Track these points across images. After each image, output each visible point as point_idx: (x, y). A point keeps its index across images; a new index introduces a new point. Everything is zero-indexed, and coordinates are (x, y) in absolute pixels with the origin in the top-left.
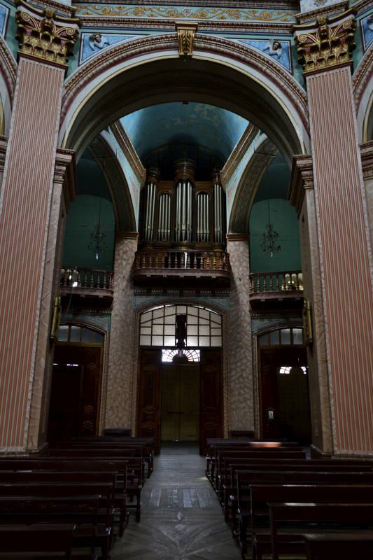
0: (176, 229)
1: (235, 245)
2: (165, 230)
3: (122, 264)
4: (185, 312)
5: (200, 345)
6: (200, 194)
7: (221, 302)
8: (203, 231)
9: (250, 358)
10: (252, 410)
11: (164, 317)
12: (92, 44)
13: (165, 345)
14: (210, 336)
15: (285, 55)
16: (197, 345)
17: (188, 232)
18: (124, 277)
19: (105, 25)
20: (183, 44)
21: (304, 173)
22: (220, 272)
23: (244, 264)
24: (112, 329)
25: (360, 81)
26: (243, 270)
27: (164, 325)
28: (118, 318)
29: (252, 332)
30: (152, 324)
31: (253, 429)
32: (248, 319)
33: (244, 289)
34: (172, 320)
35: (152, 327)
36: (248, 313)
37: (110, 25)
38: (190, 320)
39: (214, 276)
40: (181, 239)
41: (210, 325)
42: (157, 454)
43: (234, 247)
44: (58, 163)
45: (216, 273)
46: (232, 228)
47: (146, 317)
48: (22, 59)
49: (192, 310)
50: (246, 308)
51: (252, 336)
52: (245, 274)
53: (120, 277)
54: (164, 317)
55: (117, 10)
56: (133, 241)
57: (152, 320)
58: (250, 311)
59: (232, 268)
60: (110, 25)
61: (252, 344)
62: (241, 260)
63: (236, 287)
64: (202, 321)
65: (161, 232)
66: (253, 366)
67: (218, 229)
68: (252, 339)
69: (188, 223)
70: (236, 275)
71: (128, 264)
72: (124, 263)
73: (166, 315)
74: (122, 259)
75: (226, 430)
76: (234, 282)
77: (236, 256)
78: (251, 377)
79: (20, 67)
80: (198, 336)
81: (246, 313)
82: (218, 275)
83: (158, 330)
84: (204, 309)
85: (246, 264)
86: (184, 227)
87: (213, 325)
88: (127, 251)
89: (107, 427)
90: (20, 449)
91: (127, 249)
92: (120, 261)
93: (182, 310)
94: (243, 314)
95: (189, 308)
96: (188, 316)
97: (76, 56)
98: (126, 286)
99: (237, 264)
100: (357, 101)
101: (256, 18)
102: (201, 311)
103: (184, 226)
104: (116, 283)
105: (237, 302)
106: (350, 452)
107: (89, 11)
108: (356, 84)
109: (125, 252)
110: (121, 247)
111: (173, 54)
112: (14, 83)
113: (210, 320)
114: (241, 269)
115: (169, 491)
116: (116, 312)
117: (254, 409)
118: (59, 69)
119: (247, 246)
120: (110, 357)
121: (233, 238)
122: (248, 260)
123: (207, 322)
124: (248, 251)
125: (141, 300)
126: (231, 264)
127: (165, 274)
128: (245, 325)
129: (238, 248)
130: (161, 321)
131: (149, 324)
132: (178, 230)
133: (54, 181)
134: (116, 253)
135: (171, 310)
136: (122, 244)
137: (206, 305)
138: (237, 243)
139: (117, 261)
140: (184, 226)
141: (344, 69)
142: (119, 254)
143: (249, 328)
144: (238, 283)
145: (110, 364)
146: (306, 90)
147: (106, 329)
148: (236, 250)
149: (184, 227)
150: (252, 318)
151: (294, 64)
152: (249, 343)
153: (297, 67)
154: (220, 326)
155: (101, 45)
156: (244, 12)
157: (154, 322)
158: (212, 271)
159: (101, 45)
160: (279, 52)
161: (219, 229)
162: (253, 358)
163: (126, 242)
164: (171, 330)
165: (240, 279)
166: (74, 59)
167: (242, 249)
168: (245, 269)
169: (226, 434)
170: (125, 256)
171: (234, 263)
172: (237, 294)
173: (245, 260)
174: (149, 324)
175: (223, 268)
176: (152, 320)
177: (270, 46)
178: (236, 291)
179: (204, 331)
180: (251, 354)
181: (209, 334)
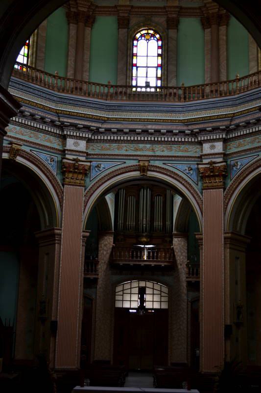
0: (139, 223)
1: (178, 240)
2: (131, 223)
3: (103, 253)
4: (144, 286)
5: (154, 307)
6: (156, 196)
7: (167, 279)
8: (158, 223)
9: (185, 317)
10: (186, 350)
11: (131, 288)
12: (96, 169)
13: (131, 307)
14: (161, 302)
15: (195, 173)
16: (152, 307)
17: (148, 225)
18: (105, 263)
19: (103, 157)
20: (143, 169)
21: (199, 241)
22: (167, 262)
23: (184, 254)
24: (98, 297)
25: (227, 197)
26: (183, 258)
27: (130, 301)
28: (101, 290)
29: (188, 300)
30: (123, 293)
31: (186, 362)
32: (185, 291)
33: (184, 271)
34: (136, 290)
35: (123, 295)
36: (185, 287)
37: (105, 157)
38: (148, 291)
39: (163, 265)
40: (143, 232)
41: (161, 294)
42: (127, 375)
43: (178, 242)
44: (84, 237)
45: (164, 262)
46: (177, 229)
47: (119, 288)
48: (65, 186)
49: (149, 284)
50: (185, 284)
51: (187, 302)
52: (184, 261)
53: (102, 263)
54: (131, 288)
55: (108, 147)
56: (111, 237)
57: (123, 290)
58: (186, 286)
59: (176, 256)
60: (105, 157)
61: (187, 308)
62: (182, 251)
63: (178, 270)
64: (155, 292)
65: (128, 225)
66: (187, 322)
67: (168, 223)
68: (187, 304)
69: (148, 219)
70: (178, 262)
71: (107, 253)
72: (105, 253)
73: (132, 287)
74: (103, 249)
75: (169, 362)
76: (177, 267)
77: (179, 248)
78: (185, 329)
79: (65, 190)
80: (153, 301)
81: (184, 288)
82: (166, 264)
83: (127, 297)
84: (157, 284)
85: (185, 254)
86: (144, 222)
87: (163, 294)
88: (106, 244)
89: (96, 359)
90: (74, 367)
91: (107, 243)
92: (102, 251)
93: (142, 284)
94: (182, 288)
95: (147, 283)
96: (147, 288)
97: (89, 175)
98: (107, 268)
99: (179, 254)
100: (226, 207)
101: (180, 151)
102: (155, 285)
103: (144, 221)
104: (99, 266)
105: (178, 279)
106: (209, 371)
107: (94, 148)
108: (225, 197)
109: (105, 245)
110: (103, 242)
111: (136, 174)
112: (62, 198)
113: (161, 291)
114: (182, 257)
115: (128, 99)
116: (100, 286)
117: (187, 349)
118: (82, 188)
119: (186, 242)
120: (97, 315)
121: (177, 236)
122: (186, 251)
123: (159, 292)
124: (186, 245)
125: (116, 278)
126: (175, 253)
127: (132, 263)
128: (183, 295)
129: (180, 242)
130: (129, 291)
131: (121, 293)
132: (140, 224)
133: (83, 246)
134: (100, 246)
135: (135, 284)
136: (103, 240)
137: (158, 281)
138: (180, 239)
139: (100, 251)
140: (144, 221)
141: (220, 190)
142: (101, 247)
143: (185, 297)
144: (179, 267)
145: (97, 319)
146: (202, 195)
147: (94, 297)
148: (179, 244)
149: (144, 222)
150: (188, 291)
151: (199, 178)
152: (185, 307)
153: (200, 180)
154: (167, 295)
155: (101, 169)
156: (175, 147)
157: (125, 292)
158: (162, 262)
159: (101, 169)
160: (191, 172)
161: (169, 224)
162: (187, 317)
163: (106, 238)
164: (135, 297)
165: (181, 265)
166: (87, 177)
167: (183, 243)
168: (184, 258)
169: (169, 365)
170: (105, 248)
171: (177, 253)
172: (179, 275)
173: (184, 252)
174: (121, 293)
175: (170, 259)
176: (123, 290)
177: (187, 169)
178: (178, 272)
179: (157, 298)
180: (186, 314)
181: (160, 300)
